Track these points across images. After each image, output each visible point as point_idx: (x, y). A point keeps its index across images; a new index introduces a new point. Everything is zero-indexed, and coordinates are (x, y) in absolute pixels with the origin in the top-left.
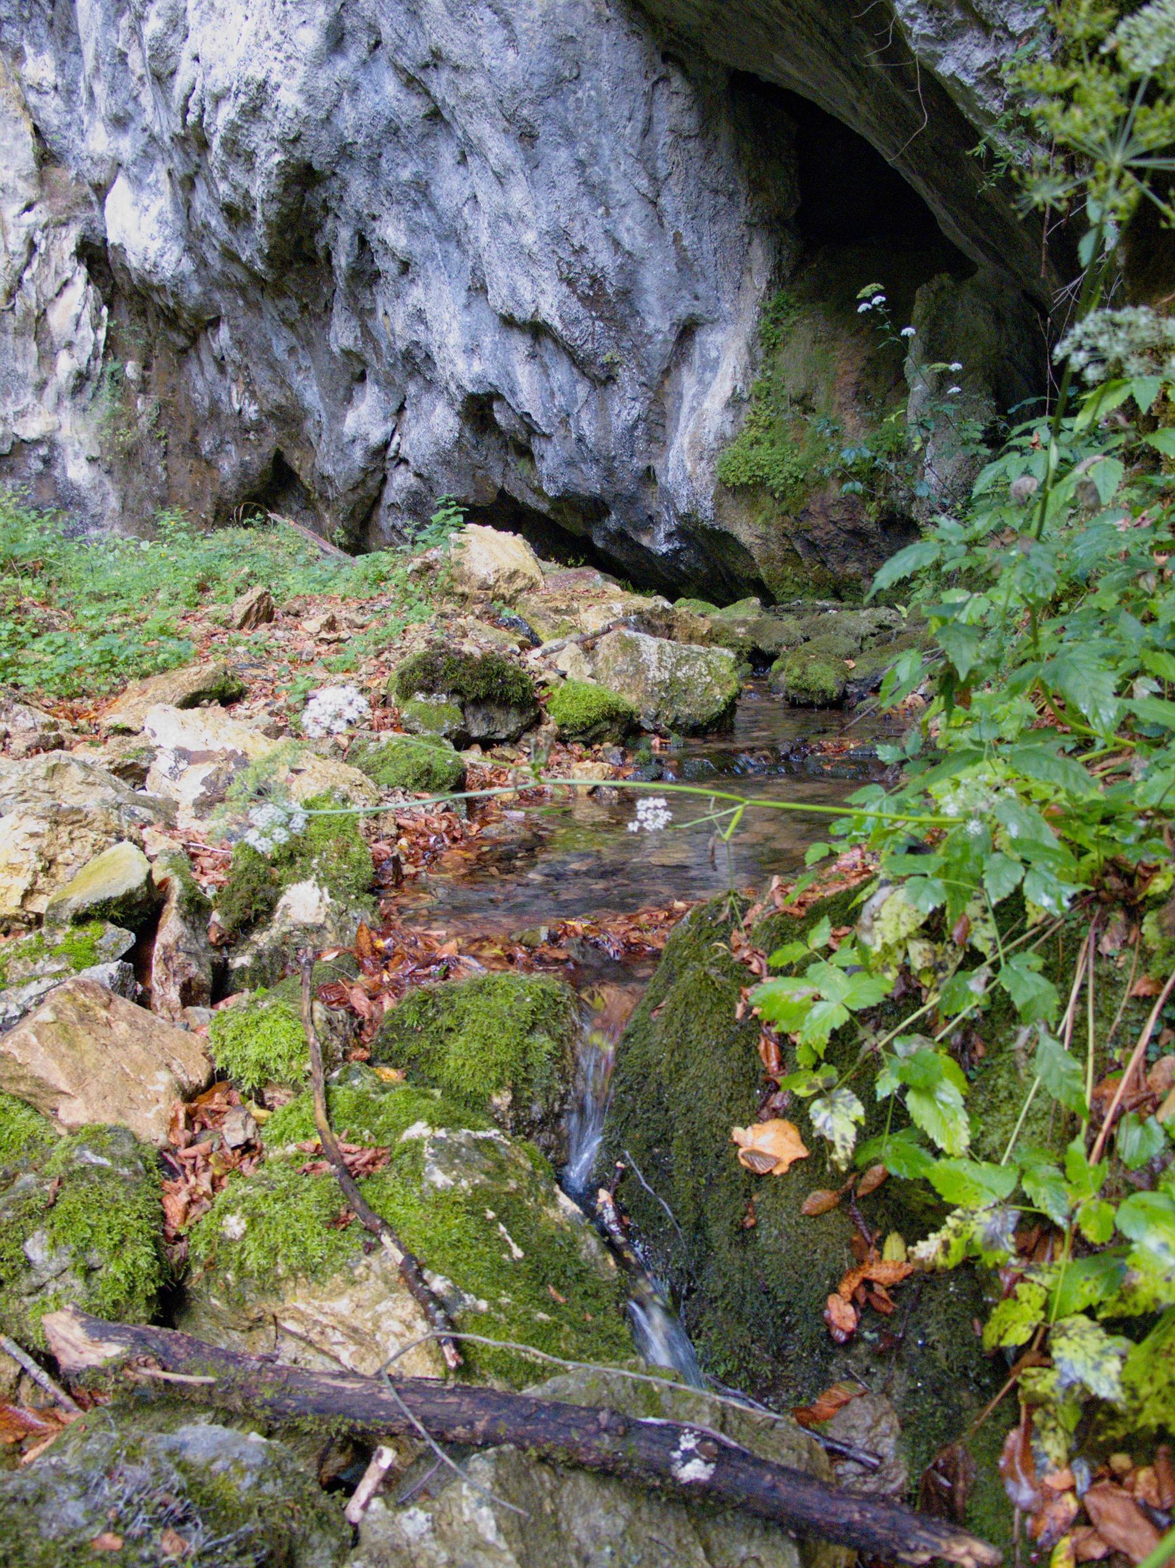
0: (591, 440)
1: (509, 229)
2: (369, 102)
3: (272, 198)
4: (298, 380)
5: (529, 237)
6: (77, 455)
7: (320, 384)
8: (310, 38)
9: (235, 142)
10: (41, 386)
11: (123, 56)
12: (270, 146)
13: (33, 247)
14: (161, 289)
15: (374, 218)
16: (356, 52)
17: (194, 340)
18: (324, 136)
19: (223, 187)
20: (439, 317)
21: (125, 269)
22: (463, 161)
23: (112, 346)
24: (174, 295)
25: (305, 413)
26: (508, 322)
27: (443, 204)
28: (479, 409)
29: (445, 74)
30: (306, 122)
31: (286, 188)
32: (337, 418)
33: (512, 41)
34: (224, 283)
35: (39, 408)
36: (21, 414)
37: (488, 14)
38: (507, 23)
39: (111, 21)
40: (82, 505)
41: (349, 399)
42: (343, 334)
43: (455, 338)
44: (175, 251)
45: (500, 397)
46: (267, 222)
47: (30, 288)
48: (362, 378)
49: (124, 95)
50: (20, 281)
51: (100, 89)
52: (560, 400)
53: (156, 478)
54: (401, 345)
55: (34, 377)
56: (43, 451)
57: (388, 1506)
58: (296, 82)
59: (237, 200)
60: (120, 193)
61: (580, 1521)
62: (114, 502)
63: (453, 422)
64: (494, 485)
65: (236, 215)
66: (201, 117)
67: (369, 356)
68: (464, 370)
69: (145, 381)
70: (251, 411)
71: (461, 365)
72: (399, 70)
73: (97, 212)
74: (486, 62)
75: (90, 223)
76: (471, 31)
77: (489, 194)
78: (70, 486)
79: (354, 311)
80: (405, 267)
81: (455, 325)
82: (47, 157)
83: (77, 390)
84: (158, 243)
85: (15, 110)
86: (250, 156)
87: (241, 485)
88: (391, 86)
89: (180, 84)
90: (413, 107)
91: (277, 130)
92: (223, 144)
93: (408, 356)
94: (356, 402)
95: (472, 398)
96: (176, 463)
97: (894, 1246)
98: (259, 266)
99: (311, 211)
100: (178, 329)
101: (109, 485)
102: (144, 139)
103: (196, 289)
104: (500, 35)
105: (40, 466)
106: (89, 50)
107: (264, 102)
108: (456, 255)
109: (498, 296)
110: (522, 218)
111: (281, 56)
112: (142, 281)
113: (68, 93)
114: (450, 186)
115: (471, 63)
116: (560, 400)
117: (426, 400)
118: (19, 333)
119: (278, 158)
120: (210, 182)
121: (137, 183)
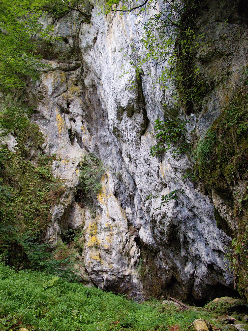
1: (211, 234)
2: (183, 214)
3: (168, 230)
5: (215, 235)
6: (135, 278)
7: (180, 262)
9: (161, 222)
10: (128, 265)
11: (142, 208)
12: (166, 222)
13: (127, 240)
14: (149, 246)
15: (186, 232)
16: (180, 206)
17: (156, 255)
18: (176, 220)
19: (159, 229)
21: (143, 242)
22: (201, 222)
23: (141, 256)
24: (152, 247)
25: (178, 268)
26: (213, 250)
27: (198, 229)
28: (211, 266)
29: (196, 209)
30: (173, 218)
31: (170, 228)
32: (184, 268)
33: (206, 203)
35: (128, 269)
36: (125, 270)
37: (202, 200)
38: (205, 200)
39: (140, 203)
40: (136, 287)
41: (185, 265)
42: (183, 253)
43: (204, 253)
44: (151, 239)
45: (215, 264)
46: (167, 234)
47: (127, 247)
48: (187, 261)
49: (142, 214)
50: (125, 247)
51: (138, 213)
53: (150, 281)
54: (194, 255)
55: (127, 263)
56: (129, 277)
57: (174, 49)
58: (170, 212)
59: (162, 231)
60: (142, 229)
61: (165, 229)
62: (142, 286)
63: (206, 269)
64: (216, 281)
65: (162, 233)
66: (155, 218)
67: (188, 256)
68: (206, 259)
69: (147, 262)
70: (167, 267)
71: (206, 258)
72: (188, 208)
73: (138, 233)
74: (202, 207)
76: (199, 202)
77: (206, 228)
78: (134, 283)
79: (185, 249)
80: (193, 241)
81: (204, 251)
82: (130, 224)
83: (135, 265)
84: (149, 238)
85: (125, 218)
86: (164, 224)
87: (166, 282)
88: (187, 211)
89: (151, 213)
90: (191, 214)
91: (168, 220)
92: (159, 222)
93: (196, 256)
94: (187, 265)
95: (209, 265)
96: (153, 278)
98: (167, 242)
99: (175, 232)
100: (153, 252)
101: (141, 283)
102: (145, 221)
103: (156, 246)
104: (204, 202)
105: (128, 280)
106: (136, 207)
107: (165, 215)
108: (202, 238)
109: (211, 245)
110: (213, 232)
111: (168, 208)
112: (146, 244)
113: (133, 214)
114: (199, 226)
115: (200, 207)
117: (200, 265)
118: (125, 256)
119: (168, 224)
120: (157, 228)
121: (145, 228)
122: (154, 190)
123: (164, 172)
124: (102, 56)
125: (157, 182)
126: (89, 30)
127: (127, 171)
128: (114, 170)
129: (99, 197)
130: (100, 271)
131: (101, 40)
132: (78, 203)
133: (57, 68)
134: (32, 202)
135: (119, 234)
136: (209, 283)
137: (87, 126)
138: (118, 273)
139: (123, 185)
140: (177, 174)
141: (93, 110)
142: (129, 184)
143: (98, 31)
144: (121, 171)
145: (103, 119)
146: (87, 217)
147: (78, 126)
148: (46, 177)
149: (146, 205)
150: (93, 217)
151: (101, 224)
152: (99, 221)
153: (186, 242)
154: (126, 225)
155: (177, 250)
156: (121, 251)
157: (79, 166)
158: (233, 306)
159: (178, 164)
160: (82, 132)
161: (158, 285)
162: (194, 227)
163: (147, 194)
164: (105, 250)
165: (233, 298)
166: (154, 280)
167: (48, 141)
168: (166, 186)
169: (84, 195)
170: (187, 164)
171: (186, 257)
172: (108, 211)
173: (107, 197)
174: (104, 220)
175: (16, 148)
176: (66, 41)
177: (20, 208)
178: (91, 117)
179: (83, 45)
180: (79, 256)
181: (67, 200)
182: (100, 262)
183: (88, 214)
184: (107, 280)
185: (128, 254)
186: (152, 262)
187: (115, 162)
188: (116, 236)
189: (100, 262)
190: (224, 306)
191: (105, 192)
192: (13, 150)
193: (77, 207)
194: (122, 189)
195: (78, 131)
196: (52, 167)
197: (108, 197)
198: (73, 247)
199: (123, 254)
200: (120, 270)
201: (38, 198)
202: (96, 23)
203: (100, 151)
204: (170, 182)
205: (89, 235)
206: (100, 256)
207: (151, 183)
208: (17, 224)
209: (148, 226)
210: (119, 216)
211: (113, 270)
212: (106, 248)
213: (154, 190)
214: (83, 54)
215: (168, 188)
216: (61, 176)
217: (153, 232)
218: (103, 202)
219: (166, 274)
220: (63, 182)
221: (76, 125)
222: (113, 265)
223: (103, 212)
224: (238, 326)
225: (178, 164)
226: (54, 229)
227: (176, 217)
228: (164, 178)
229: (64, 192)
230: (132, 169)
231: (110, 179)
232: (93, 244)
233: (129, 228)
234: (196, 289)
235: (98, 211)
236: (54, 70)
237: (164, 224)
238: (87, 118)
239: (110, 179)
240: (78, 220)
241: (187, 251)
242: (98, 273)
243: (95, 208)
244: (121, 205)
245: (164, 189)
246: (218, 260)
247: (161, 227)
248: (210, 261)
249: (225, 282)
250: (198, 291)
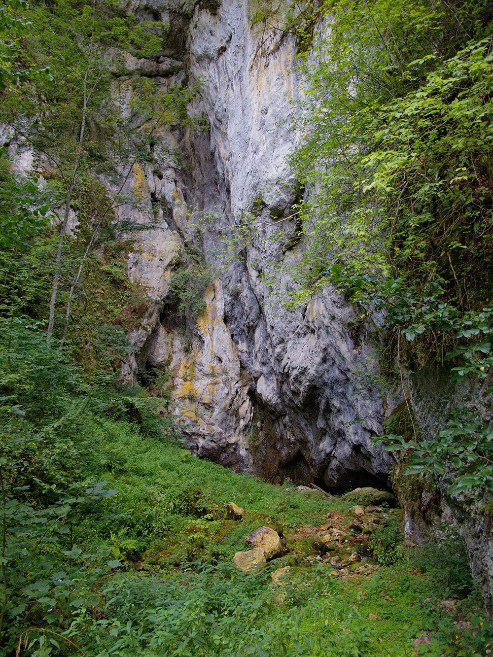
0: (386, 460)
3: (305, 392)
4: (307, 433)
5: (370, 412)
8: (318, 360)
11: (267, 350)
13: (237, 392)
16: (329, 363)
17: (278, 418)
19: (292, 387)
20: (343, 420)
23: (254, 419)
26: (365, 429)
27: (349, 398)
28: (357, 448)
30: (316, 377)
31: (309, 390)
32: (318, 444)
34: (289, 406)
36: (230, 436)
40: (242, 461)
42: (321, 423)
48: (325, 434)
51: (259, 355)
52: (378, 449)
54: (336, 429)
56: (234, 446)
58: (314, 368)
59: (296, 390)
60: (262, 380)
61: (302, 389)
62: (251, 461)
63: (350, 450)
65: (295, 393)
67: (328, 429)
69: (262, 427)
70: (293, 439)
71: (353, 437)
72: (339, 369)
75: (251, 385)
78: (240, 456)
80: (339, 411)
82: (243, 367)
83: (244, 430)
84: (271, 395)
85: (237, 358)
88: (337, 372)
89: (283, 363)
92: (294, 378)
93: (338, 432)
97: (195, 537)
98: (300, 405)
100: (274, 415)
101: (250, 456)
103: (281, 407)
113: (249, 353)
116: (378, 449)
117: (343, 443)
118: (231, 415)
119: (308, 384)
121: (267, 379)
122: (294, 332)
123: (315, 314)
124: (233, 89)
125: (300, 323)
126: (213, 29)
127: (252, 290)
128: (228, 280)
129: (201, 322)
130: (194, 434)
131: (236, 60)
132: (164, 326)
133: (137, 70)
134: (102, 323)
135: (226, 382)
136: (351, 468)
137: (183, 190)
138: (220, 439)
139: (240, 308)
140: (333, 324)
141: (197, 165)
142: (251, 308)
143: (231, 38)
144: (239, 284)
145: (217, 188)
146: (176, 350)
147: (169, 189)
148: (118, 281)
149: (278, 350)
150: (187, 350)
151: (201, 365)
152: (198, 360)
153: (328, 410)
154: (238, 369)
155: (312, 420)
156: (228, 407)
157: (169, 265)
158: (377, 499)
159: (337, 312)
160: (174, 200)
161: (274, 461)
162: (344, 395)
163: (282, 336)
164: (204, 404)
165: (379, 489)
166: (270, 454)
167: (120, 214)
168: (313, 332)
169: (175, 314)
170: (351, 317)
171: (325, 430)
172: (212, 346)
173: (212, 322)
174: (205, 359)
175: (78, 231)
176: (157, 16)
177: (87, 333)
178: (192, 176)
179: (197, 47)
180: (165, 410)
181: (151, 321)
182: (196, 422)
183: (178, 344)
184: (203, 447)
185: (236, 413)
186: (270, 428)
187: (231, 268)
188: (222, 385)
189: (196, 422)
190: (367, 499)
191: (210, 314)
192: (72, 234)
193: (162, 331)
194: (236, 312)
195: (167, 198)
196: (126, 263)
197: (215, 323)
198: (155, 395)
199: (230, 412)
200: (224, 436)
201: (109, 316)
202: (228, 22)
203: (205, 241)
204: (321, 330)
205: (181, 380)
206: (196, 413)
207: (291, 322)
208: (84, 359)
209: (273, 377)
210: (228, 355)
211: (214, 435)
212: (206, 402)
213: (294, 332)
214: (194, 65)
215: (316, 336)
216: (142, 280)
217: (280, 388)
218: (207, 330)
219: (289, 447)
220: (145, 291)
221: (163, 185)
222: (214, 428)
223: (205, 347)
224: (489, 438)
225: (337, 312)
226: (130, 366)
227: (321, 377)
228: (313, 322)
229: (147, 309)
230: (260, 290)
231: (220, 294)
232: (187, 393)
233: (241, 375)
234: (330, 473)
235: (196, 342)
236: (130, 74)
237: (300, 382)
238: (185, 175)
239: (220, 294)
240: (161, 351)
241: (327, 423)
242: (190, 436)
243: (193, 340)
244: (232, 336)
245: (308, 335)
246: (368, 442)
247: (296, 385)
248: (357, 441)
249: (372, 469)
250: (332, 476)
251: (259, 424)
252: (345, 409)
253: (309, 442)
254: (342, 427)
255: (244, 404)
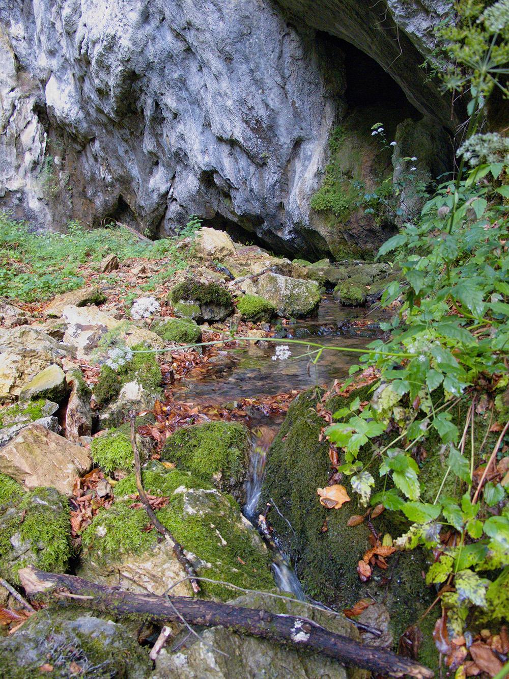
0: (256, 191)
3: (118, 86)
5: (229, 103)
11: (53, 24)
13: (14, 107)
16: (154, 23)
26: (220, 139)
28: (207, 177)
30: (132, 53)
32: (146, 181)
34: (97, 123)
36: (9, 179)
40: (35, 219)
42: (148, 145)
48: (157, 164)
51: (43, 38)
52: (242, 173)
56: (19, 195)
58: (128, 36)
59: (103, 87)
60: (52, 83)
61: (112, 83)
62: (49, 217)
63: (197, 183)
65: (102, 93)
67: (160, 154)
69: (63, 165)
70: (109, 178)
71: (200, 158)
75: (39, 96)
78: (31, 210)
80: (176, 116)
83: (33, 169)
84: (69, 105)
88: (169, 37)
89: (78, 37)
93: (177, 154)
101: (47, 210)
103: (85, 125)
113: (30, 40)
117: (184, 173)
118: (8, 144)
119: (120, 68)
121: (59, 79)
162: (182, 82)
219: (105, 192)
237: (108, 68)
241: (158, 142)
247: (102, 75)
248: (207, 165)
251: (57, 160)
252: (187, 111)
253: (132, 179)
254: (182, 145)
255: (29, 127)
